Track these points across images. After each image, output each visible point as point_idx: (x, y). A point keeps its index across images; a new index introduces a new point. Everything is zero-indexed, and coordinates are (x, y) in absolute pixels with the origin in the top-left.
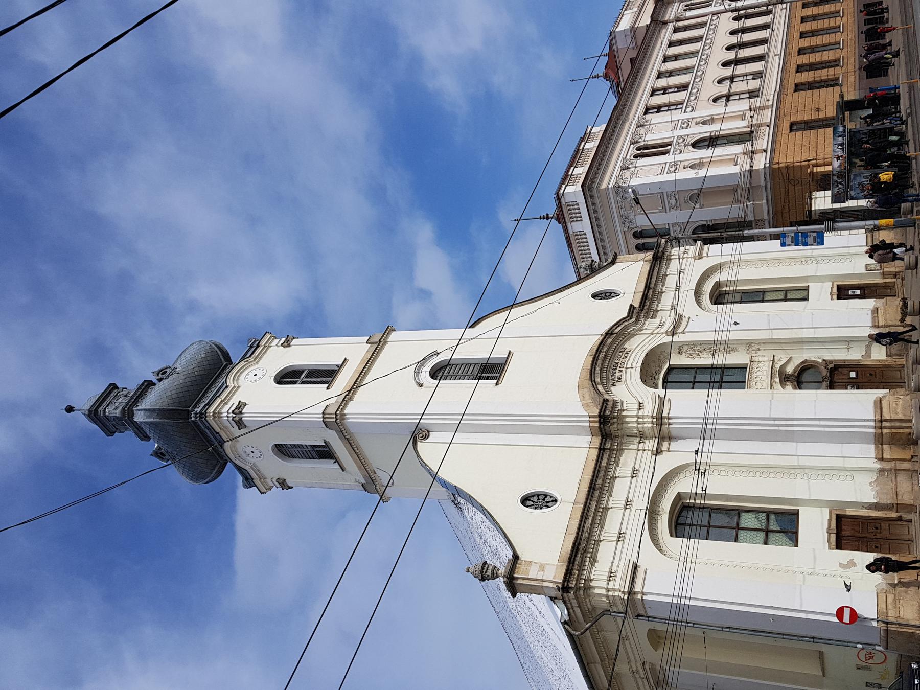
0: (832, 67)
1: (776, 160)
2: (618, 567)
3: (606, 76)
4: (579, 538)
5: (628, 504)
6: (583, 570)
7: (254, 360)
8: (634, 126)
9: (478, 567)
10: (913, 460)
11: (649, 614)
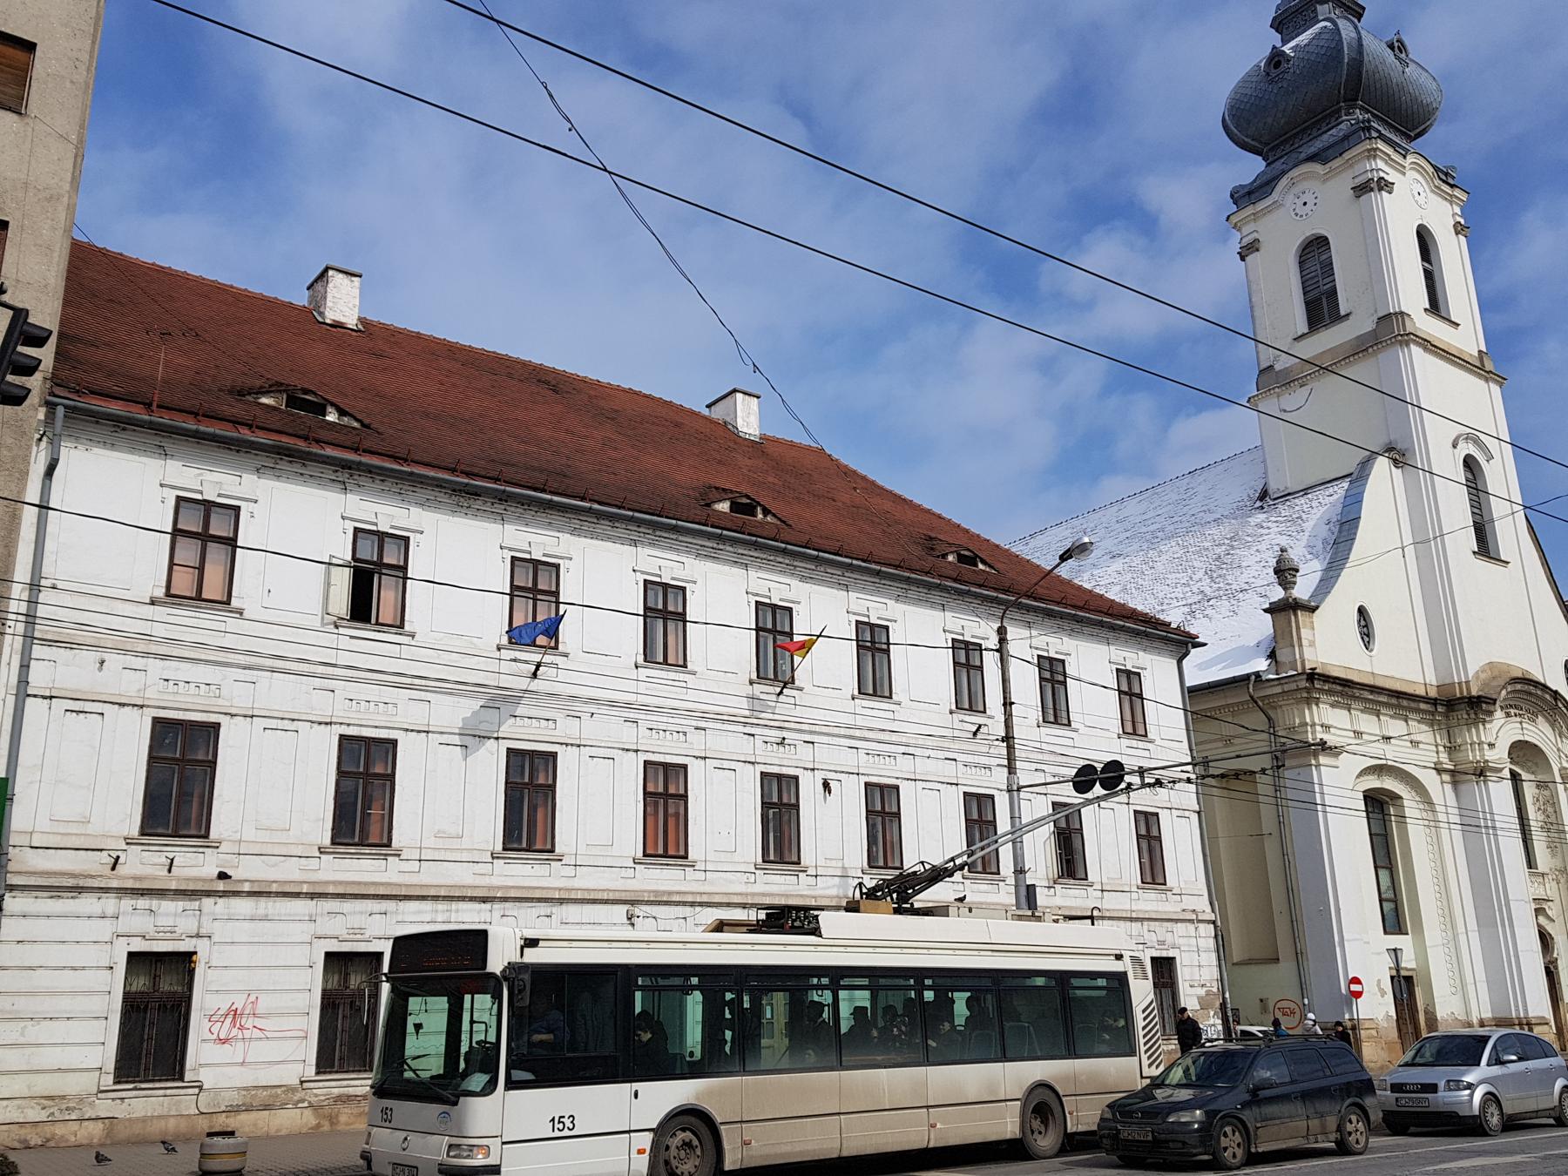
2: (1334, 734)
7: (1436, 186)
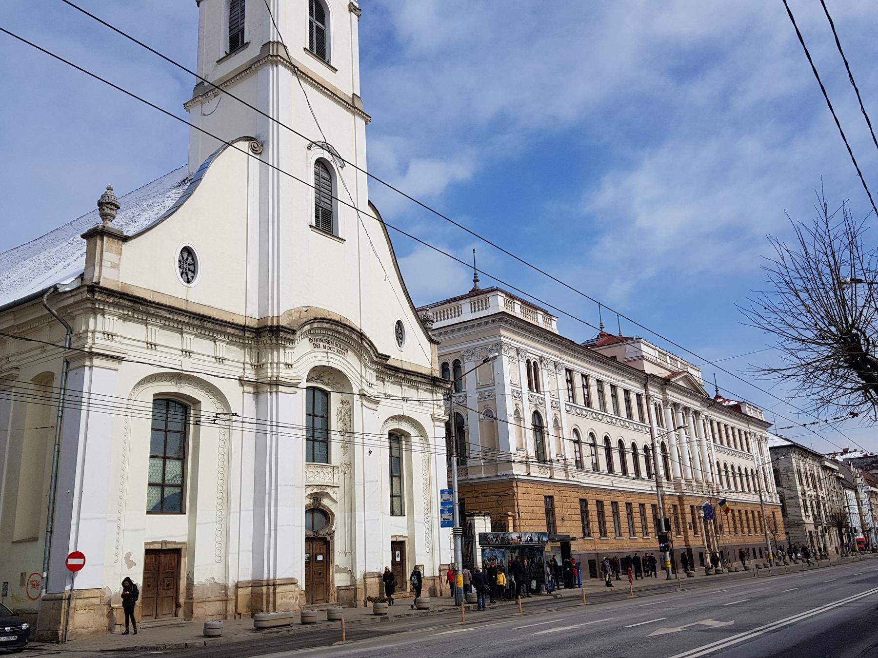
1: (520, 484)
2: (119, 342)
3: (602, 335)
4: (149, 304)
5: (187, 353)
10: (236, 614)
11: (70, 373)
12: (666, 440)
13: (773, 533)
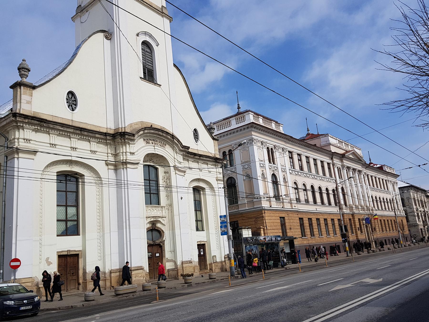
0: (311, 233)
1: (266, 212)
3: (308, 134)
4: (49, 122)
5: (74, 149)
6: (29, 125)
8: (283, 146)
9: (26, 66)
10: (111, 287)
11: (8, 162)
12: (344, 186)
13: (402, 230)
